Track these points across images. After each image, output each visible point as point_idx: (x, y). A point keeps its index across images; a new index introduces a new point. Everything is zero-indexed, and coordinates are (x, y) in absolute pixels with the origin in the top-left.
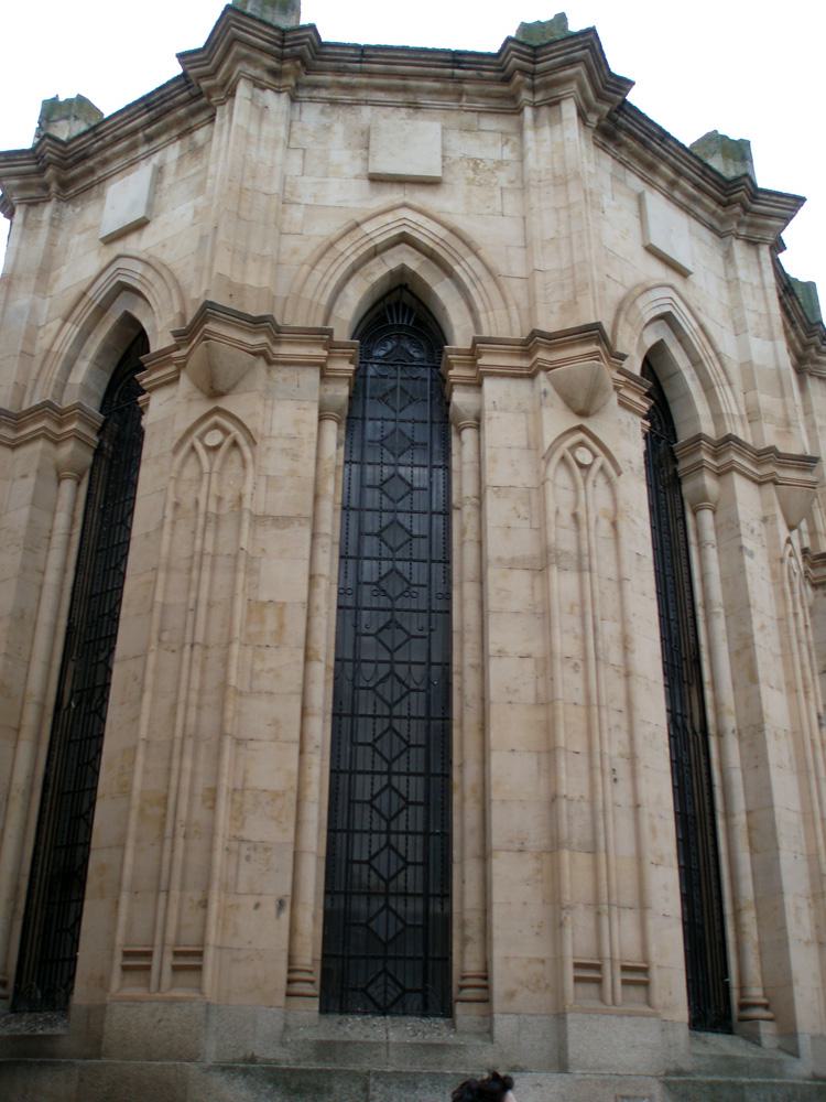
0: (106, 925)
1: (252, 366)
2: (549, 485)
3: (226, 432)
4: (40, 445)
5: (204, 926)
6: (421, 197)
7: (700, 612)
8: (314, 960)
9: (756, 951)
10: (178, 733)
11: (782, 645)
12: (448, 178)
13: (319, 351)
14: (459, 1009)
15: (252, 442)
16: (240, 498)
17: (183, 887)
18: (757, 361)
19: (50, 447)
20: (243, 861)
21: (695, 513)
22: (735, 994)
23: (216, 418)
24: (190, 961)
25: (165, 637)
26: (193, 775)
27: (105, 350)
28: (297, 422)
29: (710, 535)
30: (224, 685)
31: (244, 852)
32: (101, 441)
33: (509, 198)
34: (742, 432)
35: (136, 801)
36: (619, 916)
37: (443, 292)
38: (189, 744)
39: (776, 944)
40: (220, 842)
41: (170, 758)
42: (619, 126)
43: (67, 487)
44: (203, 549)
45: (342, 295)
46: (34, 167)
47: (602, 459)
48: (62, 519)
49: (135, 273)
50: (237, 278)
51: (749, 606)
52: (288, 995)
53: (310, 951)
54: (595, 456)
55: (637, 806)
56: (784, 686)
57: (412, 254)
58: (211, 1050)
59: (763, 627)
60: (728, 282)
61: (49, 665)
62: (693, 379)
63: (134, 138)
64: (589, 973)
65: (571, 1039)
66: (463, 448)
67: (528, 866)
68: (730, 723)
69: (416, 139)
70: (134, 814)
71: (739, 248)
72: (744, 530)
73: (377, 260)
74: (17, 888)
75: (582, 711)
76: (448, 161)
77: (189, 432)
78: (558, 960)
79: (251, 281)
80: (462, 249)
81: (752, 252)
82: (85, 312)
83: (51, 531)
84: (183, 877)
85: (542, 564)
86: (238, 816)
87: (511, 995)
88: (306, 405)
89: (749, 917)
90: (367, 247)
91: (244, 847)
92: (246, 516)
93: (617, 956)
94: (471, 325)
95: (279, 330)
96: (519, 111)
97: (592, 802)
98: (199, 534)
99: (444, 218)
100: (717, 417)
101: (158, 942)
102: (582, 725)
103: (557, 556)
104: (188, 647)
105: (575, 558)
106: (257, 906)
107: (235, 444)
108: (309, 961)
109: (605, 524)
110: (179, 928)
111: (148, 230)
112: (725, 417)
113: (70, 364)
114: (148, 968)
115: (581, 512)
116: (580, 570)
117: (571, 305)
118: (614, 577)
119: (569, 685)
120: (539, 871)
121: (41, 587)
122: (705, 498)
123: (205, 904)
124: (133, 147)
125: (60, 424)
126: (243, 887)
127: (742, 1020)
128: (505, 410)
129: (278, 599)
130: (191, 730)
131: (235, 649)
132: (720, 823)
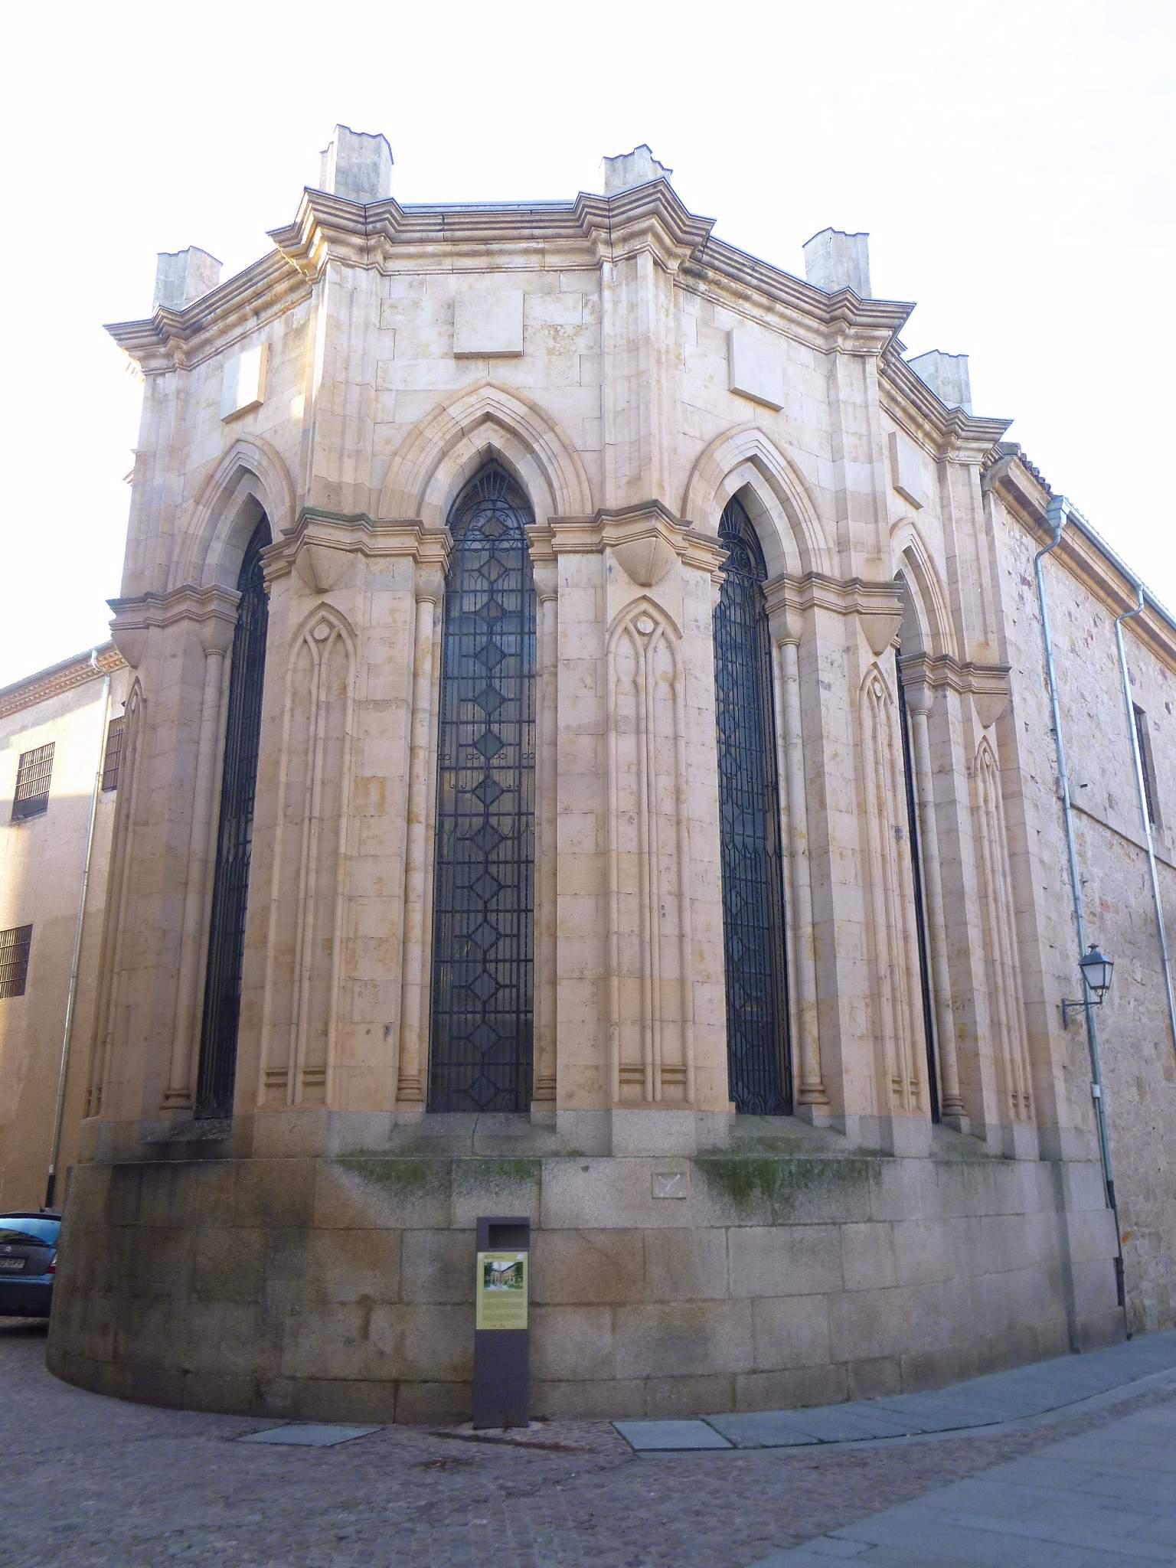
0: (257, 1051)
1: (352, 564)
2: (611, 657)
3: (331, 626)
4: (185, 625)
5: (326, 1050)
6: (504, 372)
7: (780, 742)
8: (420, 1071)
9: (815, 1046)
10: (302, 895)
11: (856, 770)
12: (530, 349)
13: (410, 542)
14: (533, 1106)
15: (353, 634)
16: (345, 687)
17: (309, 1022)
18: (850, 485)
19: (195, 626)
20: (356, 997)
21: (780, 647)
22: (796, 1082)
23: (323, 613)
24: (316, 1076)
25: (290, 811)
26: (315, 927)
27: (235, 532)
28: (393, 611)
29: (792, 669)
30: (336, 851)
31: (357, 989)
32: (240, 617)
33: (587, 365)
34: (827, 566)
35: (271, 952)
36: (662, 1029)
37: (525, 469)
38: (311, 902)
39: (830, 1042)
40: (335, 983)
41: (296, 917)
42: (700, 259)
43: (213, 662)
44: (316, 735)
45: (432, 481)
46: (155, 338)
47: (664, 625)
48: (210, 693)
49: (254, 459)
50: (334, 478)
51: (821, 737)
52: (398, 1100)
53: (417, 1061)
54: (656, 623)
55: (681, 936)
56: (854, 807)
57: (496, 431)
58: (335, 1146)
59: (836, 755)
60: (829, 404)
61: (209, 824)
62: (780, 517)
63: (242, 312)
64: (634, 1072)
66: (544, 614)
67: (587, 990)
68: (801, 845)
69: (503, 302)
70: (270, 962)
72: (821, 664)
73: (465, 441)
74: (194, 1017)
75: (635, 858)
76: (530, 331)
77: (302, 625)
78: (608, 1066)
79: (348, 478)
80: (541, 427)
81: (855, 367)
82: (214, 495)
83: (202, 704)
84: (310, 1013)
85: (603, 728)
86: (351, 961)
88: (400, 594)
89: (810, 1016)
90: (453, 431)
91: (358, 984)
92: (350, 704)
93: (658, 1062)
94: (550, 501)
95: (374, 524)
96: (598, 266)
97: (641, 936)
98: (313, 721)
99: (525, 393)
100: (804, 553)
101: (292, 1064)
102: (635, 871)
103: (616, 722)
104: (307, 821)
105: (634, 721)
106: (368, 1032)
107: (339, 636)
108: (415, 1072)
109: (664, 687)
110: (308, 1053)
111: (262, 412)
112: (812, 554)
113: (206, 548)
114: (285, 1085)
115: (641, 681)
116: (638, 732)
117: (635, 480)
118: (671, 735)
119: (623, 836)
120: (595, 994)
121: (197, 757)
122: (788, 635)
123: (325, 1033)
124: (243, 319)
125: (202, 603)
126: (357, 1017)
127: (801, 1104)
128: (577, 586)
129: (380, 774)
130: (312, 891)
131: (344, 821)
132: (789, 934)
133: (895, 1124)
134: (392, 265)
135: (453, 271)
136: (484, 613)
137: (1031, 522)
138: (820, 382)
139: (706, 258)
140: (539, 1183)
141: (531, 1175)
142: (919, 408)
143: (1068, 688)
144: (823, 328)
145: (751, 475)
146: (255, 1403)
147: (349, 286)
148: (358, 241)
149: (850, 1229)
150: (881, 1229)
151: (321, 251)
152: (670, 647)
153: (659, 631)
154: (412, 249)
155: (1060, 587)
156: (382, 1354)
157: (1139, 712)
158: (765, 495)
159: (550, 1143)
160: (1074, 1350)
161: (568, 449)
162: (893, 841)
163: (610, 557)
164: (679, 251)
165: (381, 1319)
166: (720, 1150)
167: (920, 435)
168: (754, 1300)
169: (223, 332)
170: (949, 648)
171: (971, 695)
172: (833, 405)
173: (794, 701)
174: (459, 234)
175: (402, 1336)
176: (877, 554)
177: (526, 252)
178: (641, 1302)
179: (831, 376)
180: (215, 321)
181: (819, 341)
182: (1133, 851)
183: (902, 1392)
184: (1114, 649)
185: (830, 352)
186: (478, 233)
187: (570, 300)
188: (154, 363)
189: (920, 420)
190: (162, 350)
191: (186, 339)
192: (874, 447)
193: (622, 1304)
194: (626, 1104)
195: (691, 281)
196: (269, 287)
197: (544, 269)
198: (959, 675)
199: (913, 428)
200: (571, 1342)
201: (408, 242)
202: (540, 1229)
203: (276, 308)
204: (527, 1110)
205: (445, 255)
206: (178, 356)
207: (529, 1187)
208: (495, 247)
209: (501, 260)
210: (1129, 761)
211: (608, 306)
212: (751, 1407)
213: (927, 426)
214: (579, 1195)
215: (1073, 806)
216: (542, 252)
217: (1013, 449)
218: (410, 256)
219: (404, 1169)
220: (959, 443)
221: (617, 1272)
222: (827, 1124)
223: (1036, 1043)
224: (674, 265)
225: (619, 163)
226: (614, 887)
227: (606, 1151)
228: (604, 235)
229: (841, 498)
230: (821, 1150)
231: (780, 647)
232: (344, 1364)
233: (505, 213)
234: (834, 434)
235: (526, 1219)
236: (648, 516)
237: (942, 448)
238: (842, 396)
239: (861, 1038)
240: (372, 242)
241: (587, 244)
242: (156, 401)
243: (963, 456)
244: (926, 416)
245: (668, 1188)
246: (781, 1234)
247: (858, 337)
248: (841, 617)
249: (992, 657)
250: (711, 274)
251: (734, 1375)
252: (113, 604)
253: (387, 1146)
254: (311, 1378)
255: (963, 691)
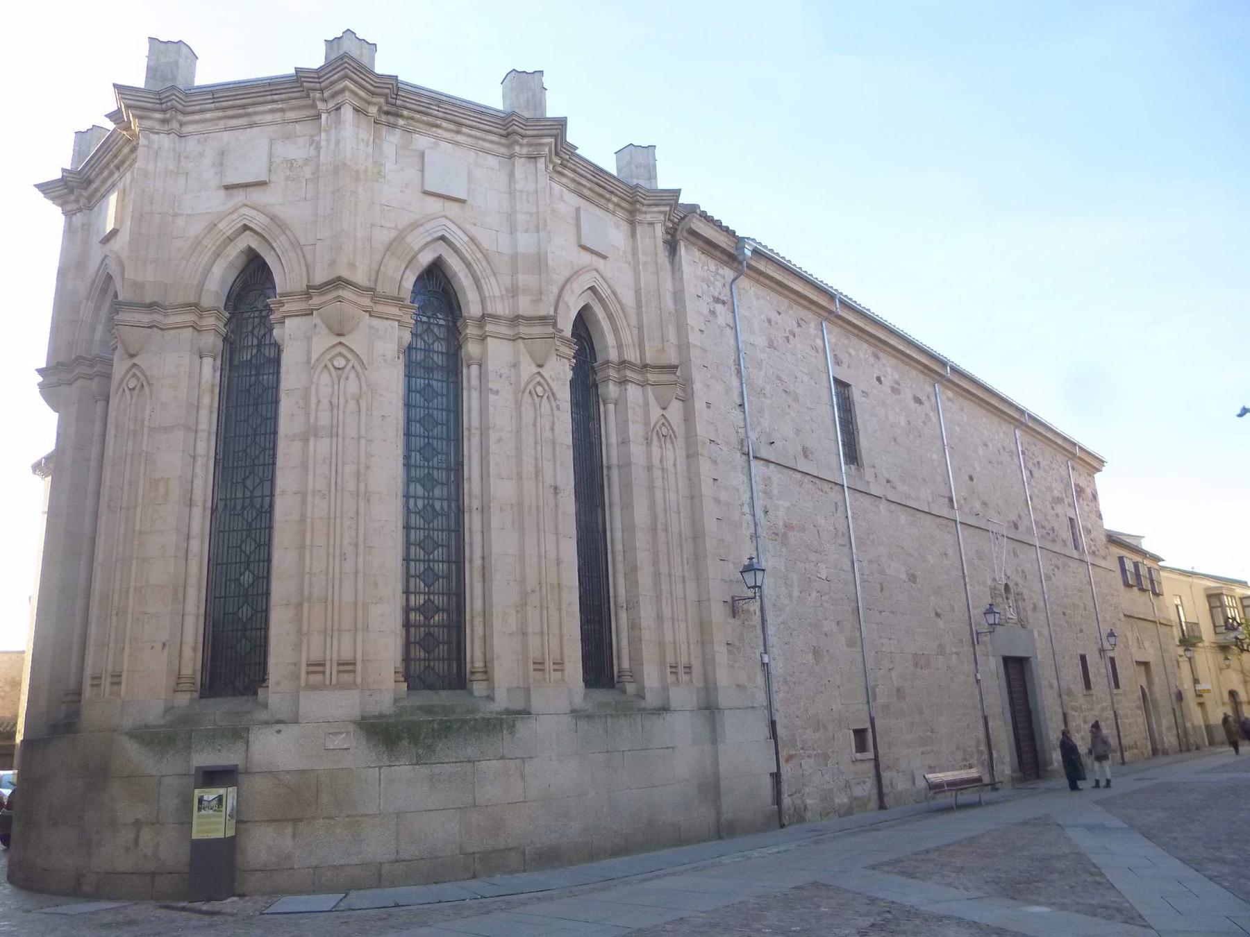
6: (257, 196)
12: (274, 178)
13: (190, 318)
22: (468, 666)
24: (116, 678)
37: (270, 260)
42: (395, 104)
47: (353, 361)
50: (140, 279)
54: (348, 360)
58: (128, 723)
59: (499, 440)
64: (317, 666)
65: (301, 705)
69: (253, 149)
71: (520, 165)
81: (531, 165)
87: (278, 683)
96: (319, 117)
97: (327, 574)
109: (352, 403)
111: (119, 236)
113: (93, 329)
117: (333, 264)
124: (111, 174)
132: (467, 565)
133: (533, 692)
134: (186, 129)
135: (226, 129)
136: (254, 361)
137: (725, 258)
138: (503, 177)
139: (399, 102)
140: (247, 743)
141: (242, 738)
142: (604, 188)
143: (762, 373)
144: (503, 141)
145: (442, 250)
146: (76, 889)
147: (156, 146)
148: (158, 115)
149: (483, 765)
150: (512, 764)
151: (135, 125)
152: (358, 376)
153: (350, 365)
154: (196, 117)
155: (755, 302)
156: (145, 856)
157: (842, 386)
158: (454, 263)
159: (264, 716)
160: (720, 837)
161: (296, 245)
162: (551, 496)
163: (316, 319)
164: (375, 100)
165: (146, 834)
166: (385, 716)
167: (611, 206)
168: (398, 815)
169: (104, 182)
170: (632, 355)
171: (649, 388)
172: (512, 193)
173: (475, 404)
174: (225, 104)
175: (158, 845)
176: (539, 295)
177: (272, 111)
178: (313, 818)
179: (511, 175)
180: (97, 176)
181: (503, 150)
182: (826, 487)
183: (524, 871)
184: (819, 342)
185: (511, 157)
186: (243, 100)
187: (301, 141)
188: (69, 207)
189: (608, 196)
190: (73, 198)
191: (85, 189)
192: (541, 222)
193: (300, 820)
194: (311, 687)
195: (391, 119)
196: (120, 151)
197: (285, 122)
198: (639, 372)
199: (603, 201)
200: (263, 844)
201: (193, 113)
202: (247, 772)
203: (127, 164)
204: (256, 693)
205: (220, 118)
206: (83, 201)
207: (240, 746)
208: (250, 110)
209: (257, 119)
210: (830, 422)
211: (323, 144)
212: (393, 884)
213: (615, 199)
214: (274, 749)
215: (756, 458)
216: (282, 110)
217: (693, 208)
218: (196, 122)
219: (159, 739)
220: (644, 209)
221: (300, 800)
222: (485, 694)
223: (704, 628)
224: (373, 110)
225: (335, 43)
226: (308, 542)
227: (295, 721)
228: (318, 95)
229: (514, 257)
230: (473, 712)
231: (469, 366)
232: (125, 863)
233: (253, 87)
234: (511, 216)
235: (236, 766)
236: (337, 288)
237: (632, 213)
238: (518, 187)
239: (511, 635)
240: (168, 116)
241: (310, 102)
242: (70, 230)
243: (649, 217)
244: (612, 192)
245: (337, 742)
246: (423, 770)
247: (530, 145)
248: (511, 343)
249: (672, 357)
250: (405, 113)
251: (381, 864)
252: (40, 371)
253: (162, 722)
254: (106, 873)
255: (643, 384)
